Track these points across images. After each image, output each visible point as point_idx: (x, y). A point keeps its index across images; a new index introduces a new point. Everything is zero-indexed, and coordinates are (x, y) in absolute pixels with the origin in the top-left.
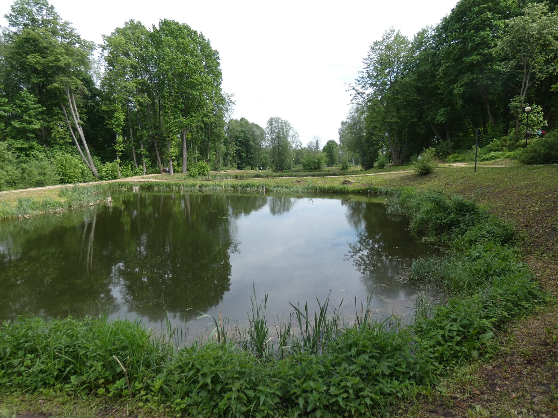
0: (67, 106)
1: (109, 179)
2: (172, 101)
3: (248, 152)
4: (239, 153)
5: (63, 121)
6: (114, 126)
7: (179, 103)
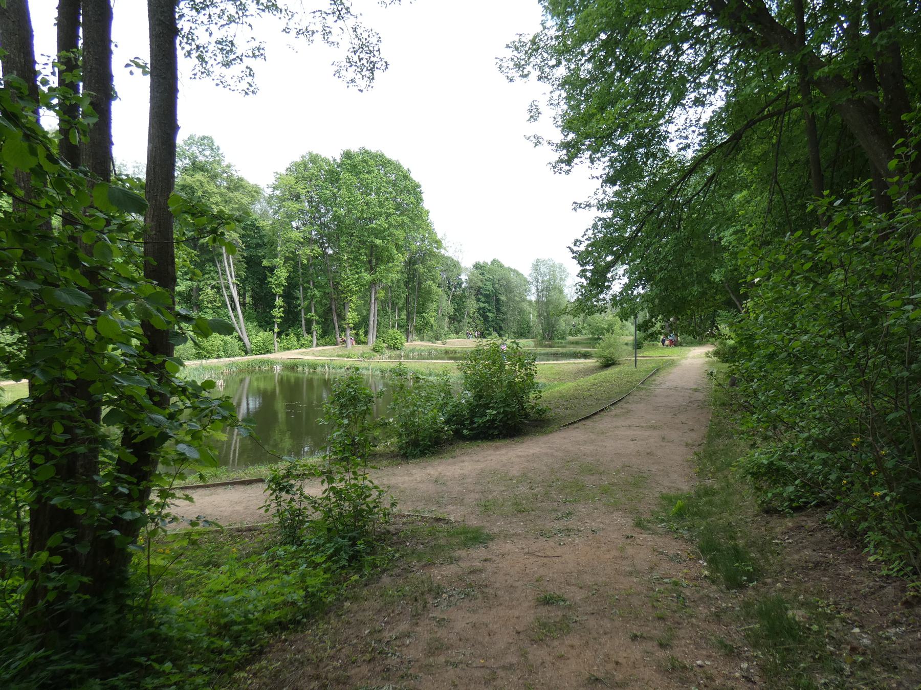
0: (221, 262)
1: (261, 354)
2: (352, 252)
3: (498, 310)
4: (484, 312)
5: (215, 280)
6: (273, 286)
7: (360, 254)
